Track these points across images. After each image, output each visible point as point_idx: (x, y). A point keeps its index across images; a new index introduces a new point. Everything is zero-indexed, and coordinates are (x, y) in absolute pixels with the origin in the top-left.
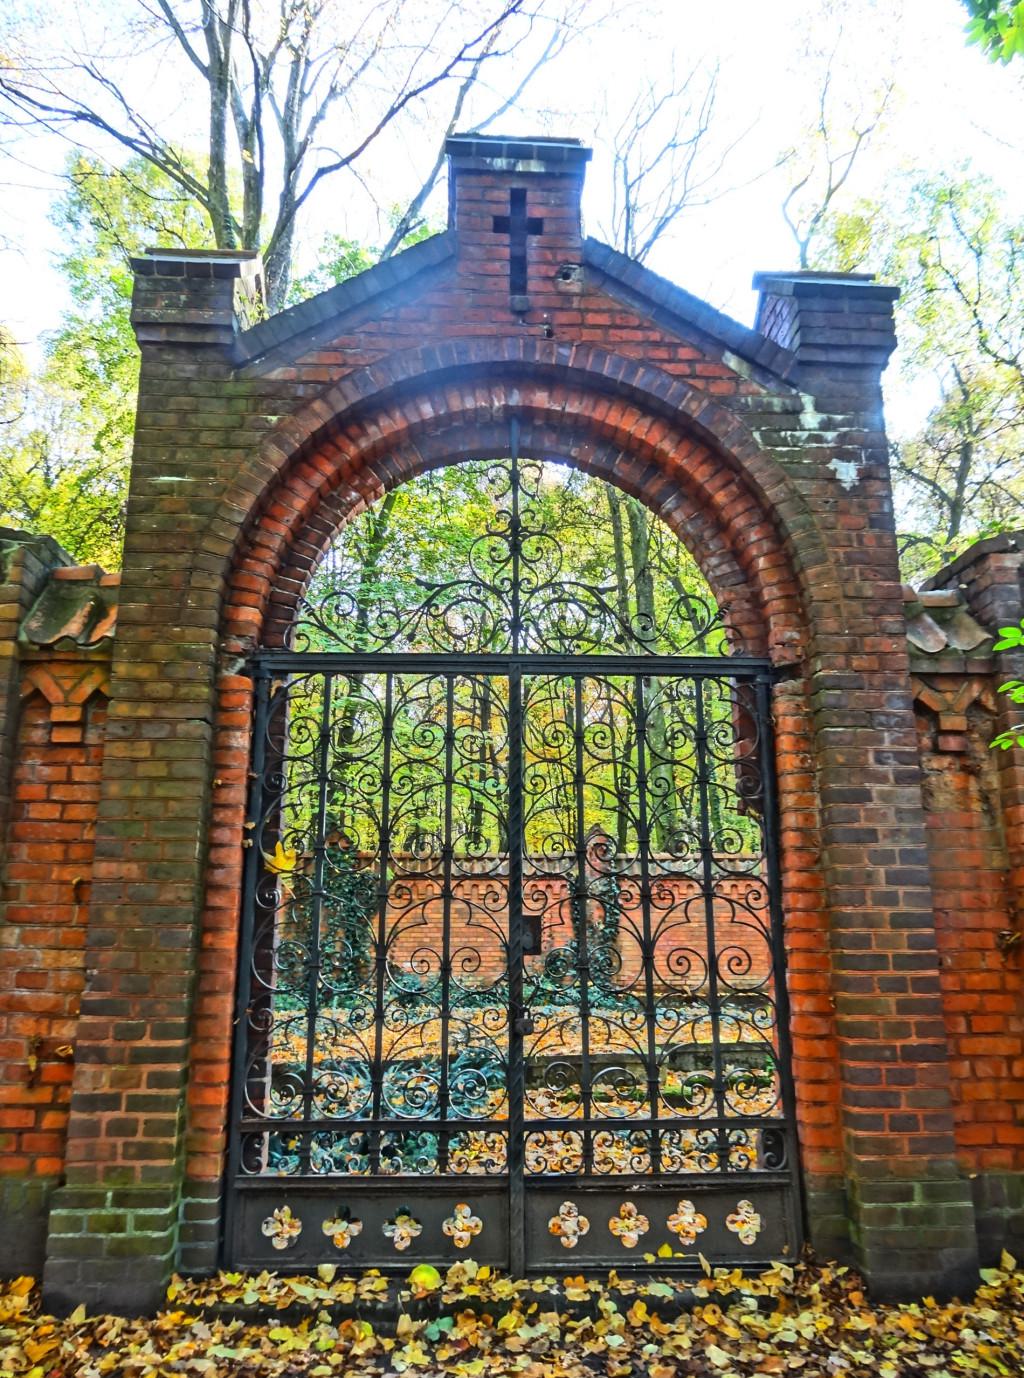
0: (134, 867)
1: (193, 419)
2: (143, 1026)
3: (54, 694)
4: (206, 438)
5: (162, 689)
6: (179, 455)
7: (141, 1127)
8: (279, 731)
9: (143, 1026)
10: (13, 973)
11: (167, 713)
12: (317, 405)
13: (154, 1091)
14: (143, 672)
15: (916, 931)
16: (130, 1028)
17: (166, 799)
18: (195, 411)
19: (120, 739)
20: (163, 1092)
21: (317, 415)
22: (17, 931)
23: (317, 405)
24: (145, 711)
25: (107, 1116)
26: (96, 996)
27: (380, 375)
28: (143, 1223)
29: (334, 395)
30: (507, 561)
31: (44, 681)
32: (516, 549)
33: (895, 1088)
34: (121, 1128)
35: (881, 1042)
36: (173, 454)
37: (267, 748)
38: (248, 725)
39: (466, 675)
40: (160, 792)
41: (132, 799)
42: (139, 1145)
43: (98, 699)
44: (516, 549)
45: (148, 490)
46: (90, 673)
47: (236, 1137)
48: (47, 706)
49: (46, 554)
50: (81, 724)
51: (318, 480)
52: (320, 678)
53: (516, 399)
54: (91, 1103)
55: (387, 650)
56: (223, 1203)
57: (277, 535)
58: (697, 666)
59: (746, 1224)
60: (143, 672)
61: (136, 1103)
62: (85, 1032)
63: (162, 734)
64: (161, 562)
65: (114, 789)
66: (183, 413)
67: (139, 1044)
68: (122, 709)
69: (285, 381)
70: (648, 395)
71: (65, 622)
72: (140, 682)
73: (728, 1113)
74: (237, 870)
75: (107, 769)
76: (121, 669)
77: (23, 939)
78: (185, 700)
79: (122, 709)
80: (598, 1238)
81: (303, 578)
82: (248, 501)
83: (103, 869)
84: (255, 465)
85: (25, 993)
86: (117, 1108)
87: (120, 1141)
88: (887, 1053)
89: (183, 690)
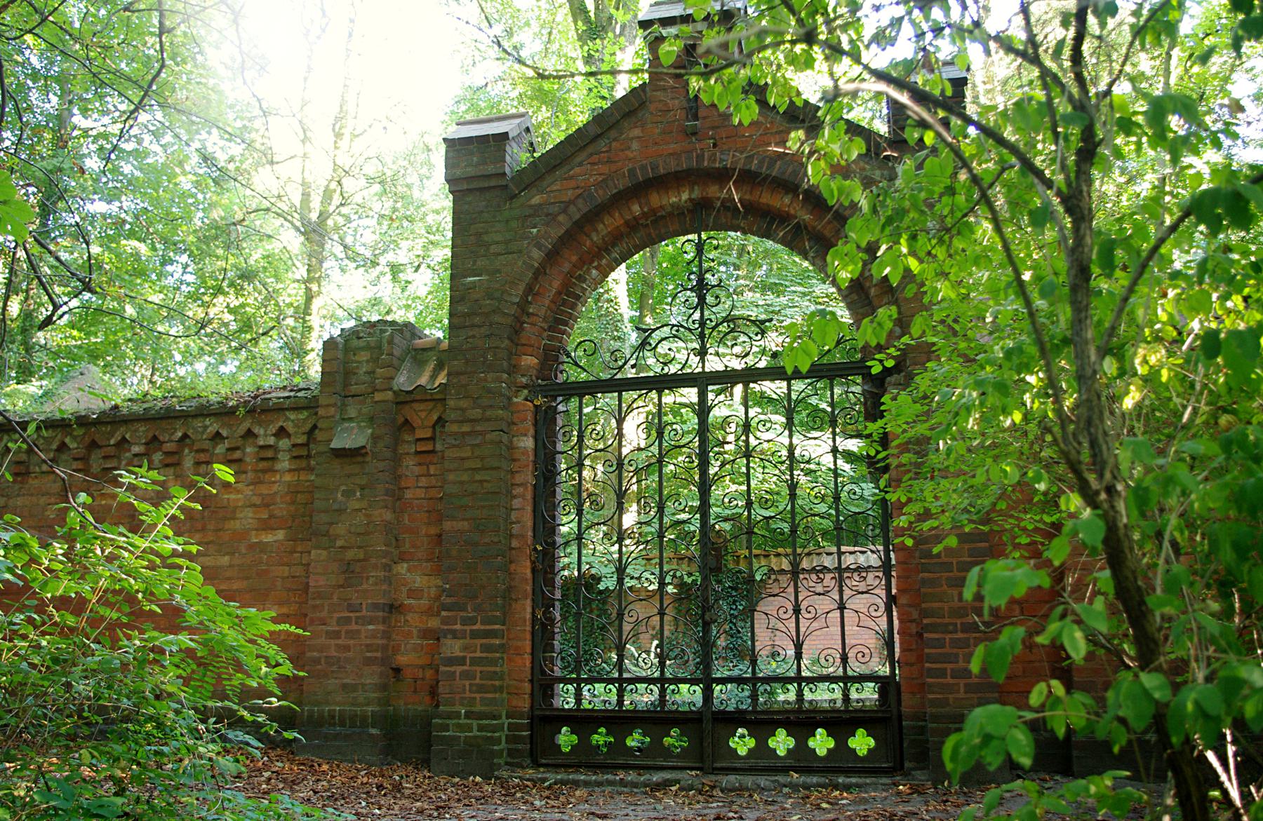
0: (466, 523)
1: (485, 238)
2: (476, 617)
3: (416, 422)
4: (493, 249)
5: (476, 413)
6: (479, 263)
7: (478, 675)
8: (552, 435)
9: (476, 617)
10: (404, 589)
11: (478, 428)
12: (561, 218)
13: (484, 655)
14: (464, 404)
15: (973, 546)
16: (470, 618)
17: (481, 482)
18: (486, 233)
19: (454, 446)
20: (490, 655)
21: (560, 224)
22: (405, 565)
23: (561, 218)
24: (466, 428)
25: (459, 669)
26: (449, 600)
27: (601, 192)
28: (481, 728)
29: (572, 209)
30: (696, 308)
31: (408, 412)
32: (702, 299)
33: (955, 651)
34: (466, 675)
35: (947, 620)
36: (475, 262)
37: (545, 447)
38: (532, 432)
39: (670, 389)
40: (478, 477)
41: (462, 483)
42: (477, 685)
43: (441, 421)
44: (702, 299)
45: (461, 288)
46: (435, 407)
47: (536, 685)
48: (413, 429)
49: (408, 335)
50: (433, 439)
51: (566, 267)
52: (654, 394)
53: (696, 194)
54: (451, 661)
55: (619, 376)
56: (531, 723)
57: (540, 308)
58: (829, 370)
59: (861, 742)
60: (464, 404)
61: (475, 662)
62: (445, 621)
63: (478, 442)
64: (471, 333)
65: (451, 477)
66: (478, 235)
67: (475, 627)
68: (454, 428)
69: (541, 205)
70: (786, 181)
71: (420, 376)
72: (463, 410)
73: (850, 673)
74: (530, 524)
75: (447, 464)
76: (451, 403)
77: (409, 570)
78: (489, 420)
79: (454, 428)
80: (762, 749)
81: (564, 332)
82: (521, 288)
83: (447, 525)
84: (524, 263)
85: (412, 601)
86: (464, 664)
87: (467, 683)
88: (951, 628)
89: (489, 413)
